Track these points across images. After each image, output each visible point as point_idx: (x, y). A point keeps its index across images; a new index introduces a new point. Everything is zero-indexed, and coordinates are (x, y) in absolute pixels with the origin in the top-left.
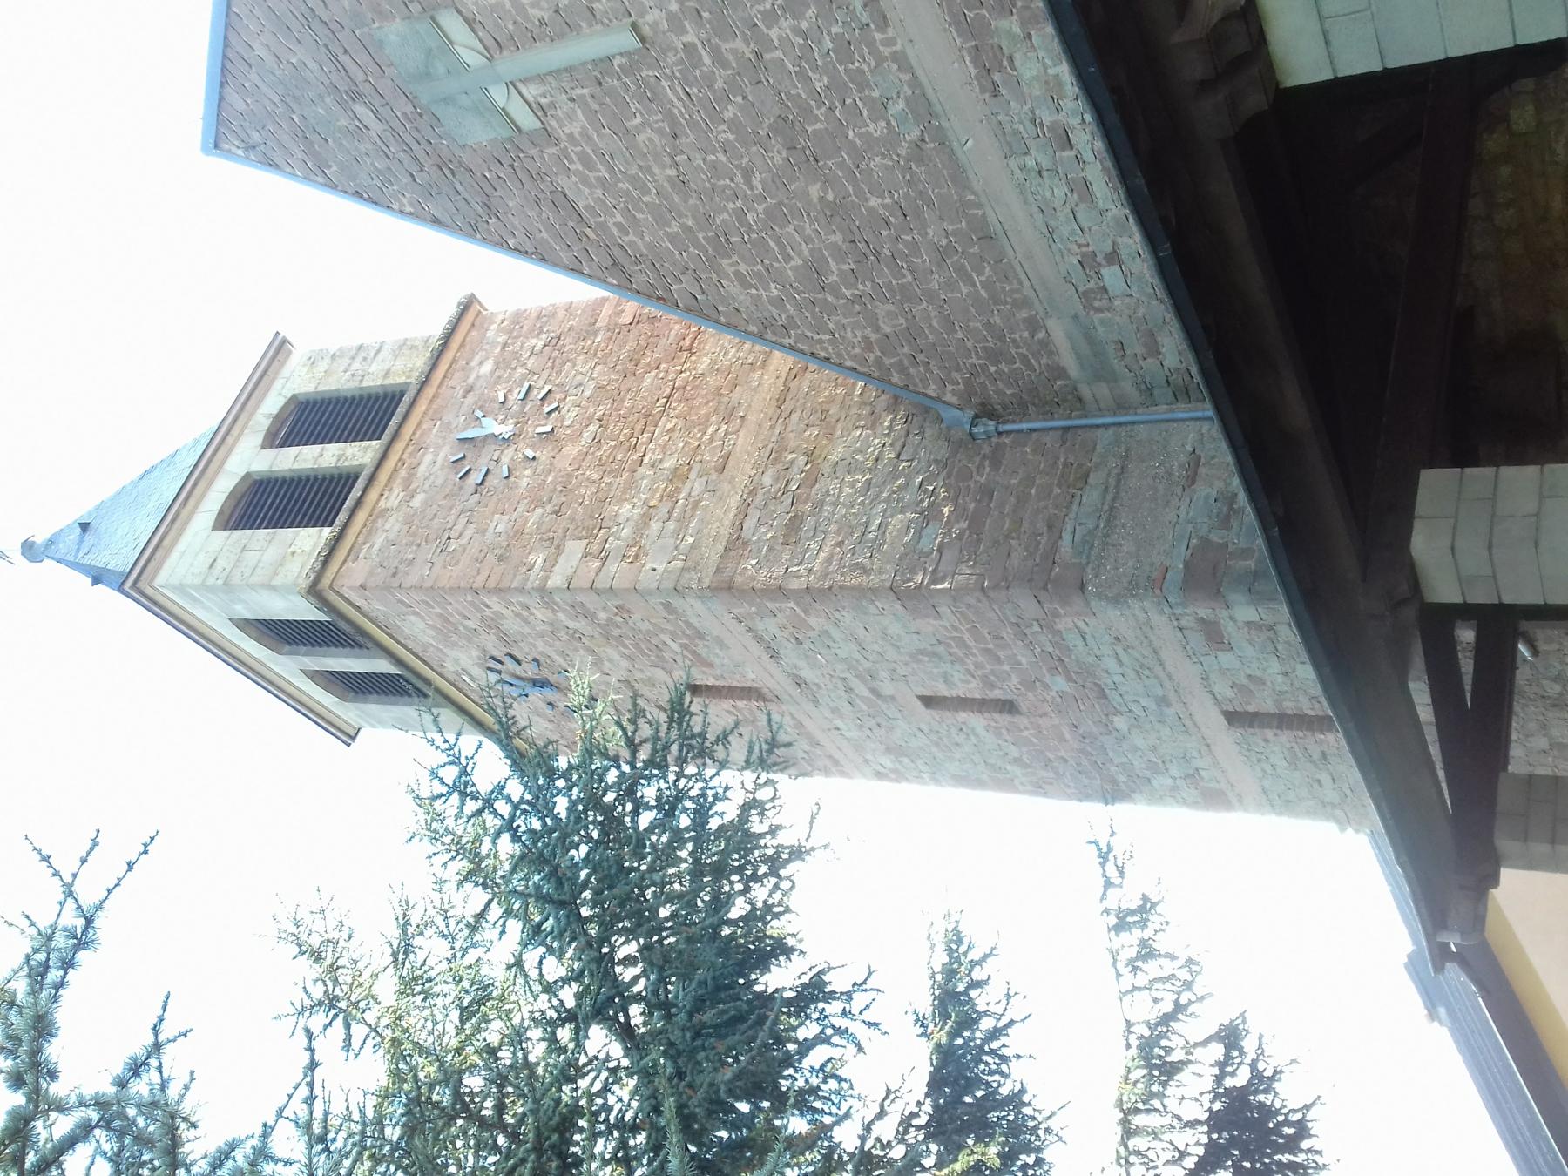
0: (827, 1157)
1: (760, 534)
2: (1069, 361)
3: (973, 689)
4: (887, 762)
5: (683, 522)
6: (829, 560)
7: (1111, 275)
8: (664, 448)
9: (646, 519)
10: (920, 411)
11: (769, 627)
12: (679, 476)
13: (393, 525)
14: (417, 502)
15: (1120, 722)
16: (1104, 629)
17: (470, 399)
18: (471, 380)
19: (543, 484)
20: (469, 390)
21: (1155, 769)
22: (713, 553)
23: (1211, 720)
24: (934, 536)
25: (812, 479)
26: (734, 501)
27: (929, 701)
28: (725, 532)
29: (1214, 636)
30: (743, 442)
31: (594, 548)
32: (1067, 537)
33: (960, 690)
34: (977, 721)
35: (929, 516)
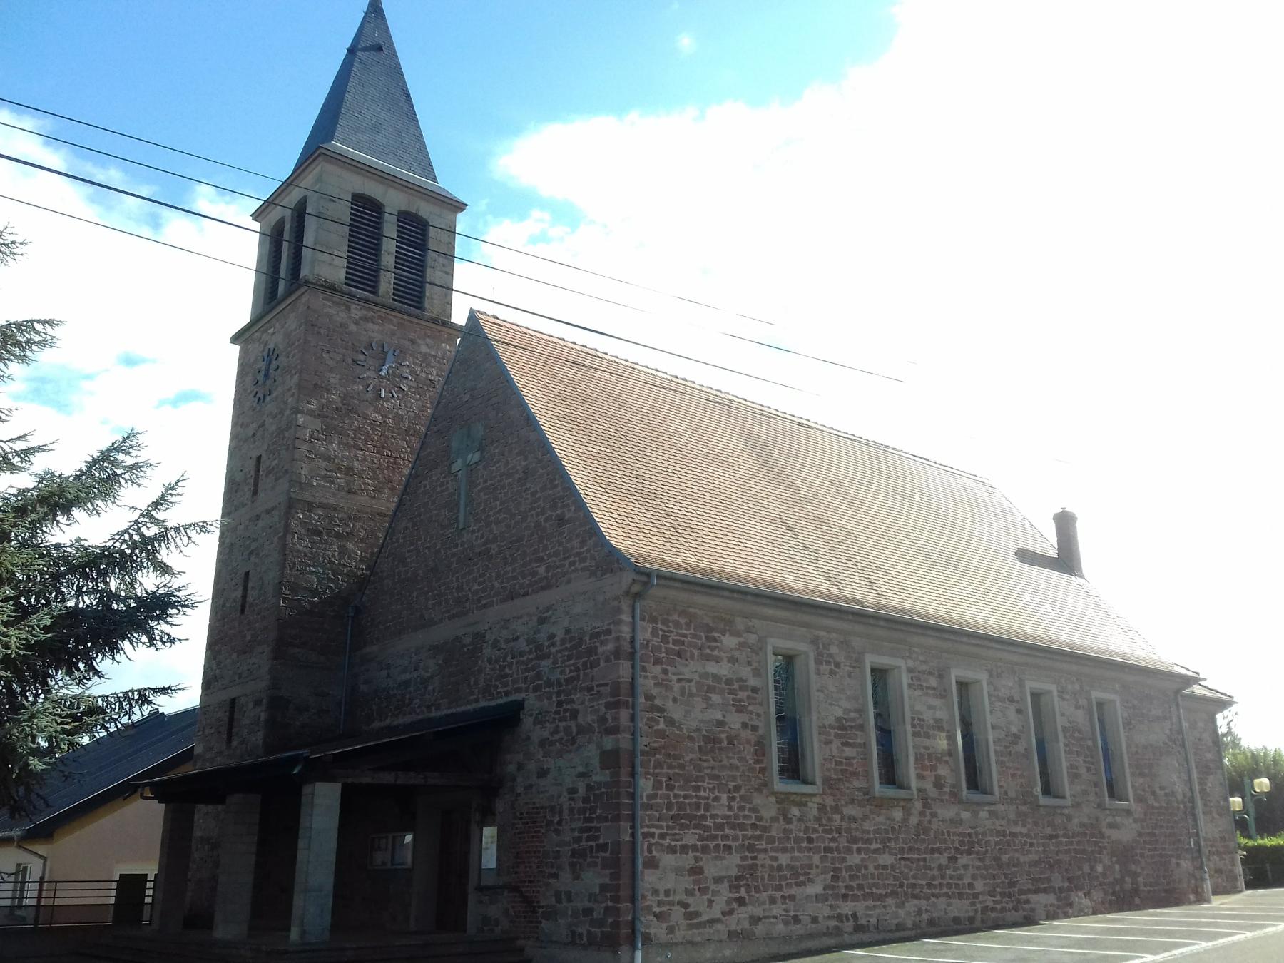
0: (28, 682)
1: (315, 518)
2: (368, 650)
3: (250, 599)
4: (227, 541)
5: (324, 478)
6: (299, 551)
7: (385, 673)
8: (364, 459)
9: (327, 458)
10: (363, 583)
11: (276, 513)
12: (349, 470)
13: (340, 315)
14: (353, 328)
15: (234, 656)
16: (261, 661)
17: (407, 343)
18: (419, 341)
19: (352, 398)
20: (413, 342)
21: (219, 664)
22: (307, 496)
23: (233, 692)
24: (303, 597)
25: (338, 536)
26: (332, 502)
27: (247, 574)
28: (317, 501)
29: (257, 703)
30: (363, 499)
31: (316, 435)
32: (297, 650)
33: (250, 592)
34: (239, 594)
35: (315, 593)
